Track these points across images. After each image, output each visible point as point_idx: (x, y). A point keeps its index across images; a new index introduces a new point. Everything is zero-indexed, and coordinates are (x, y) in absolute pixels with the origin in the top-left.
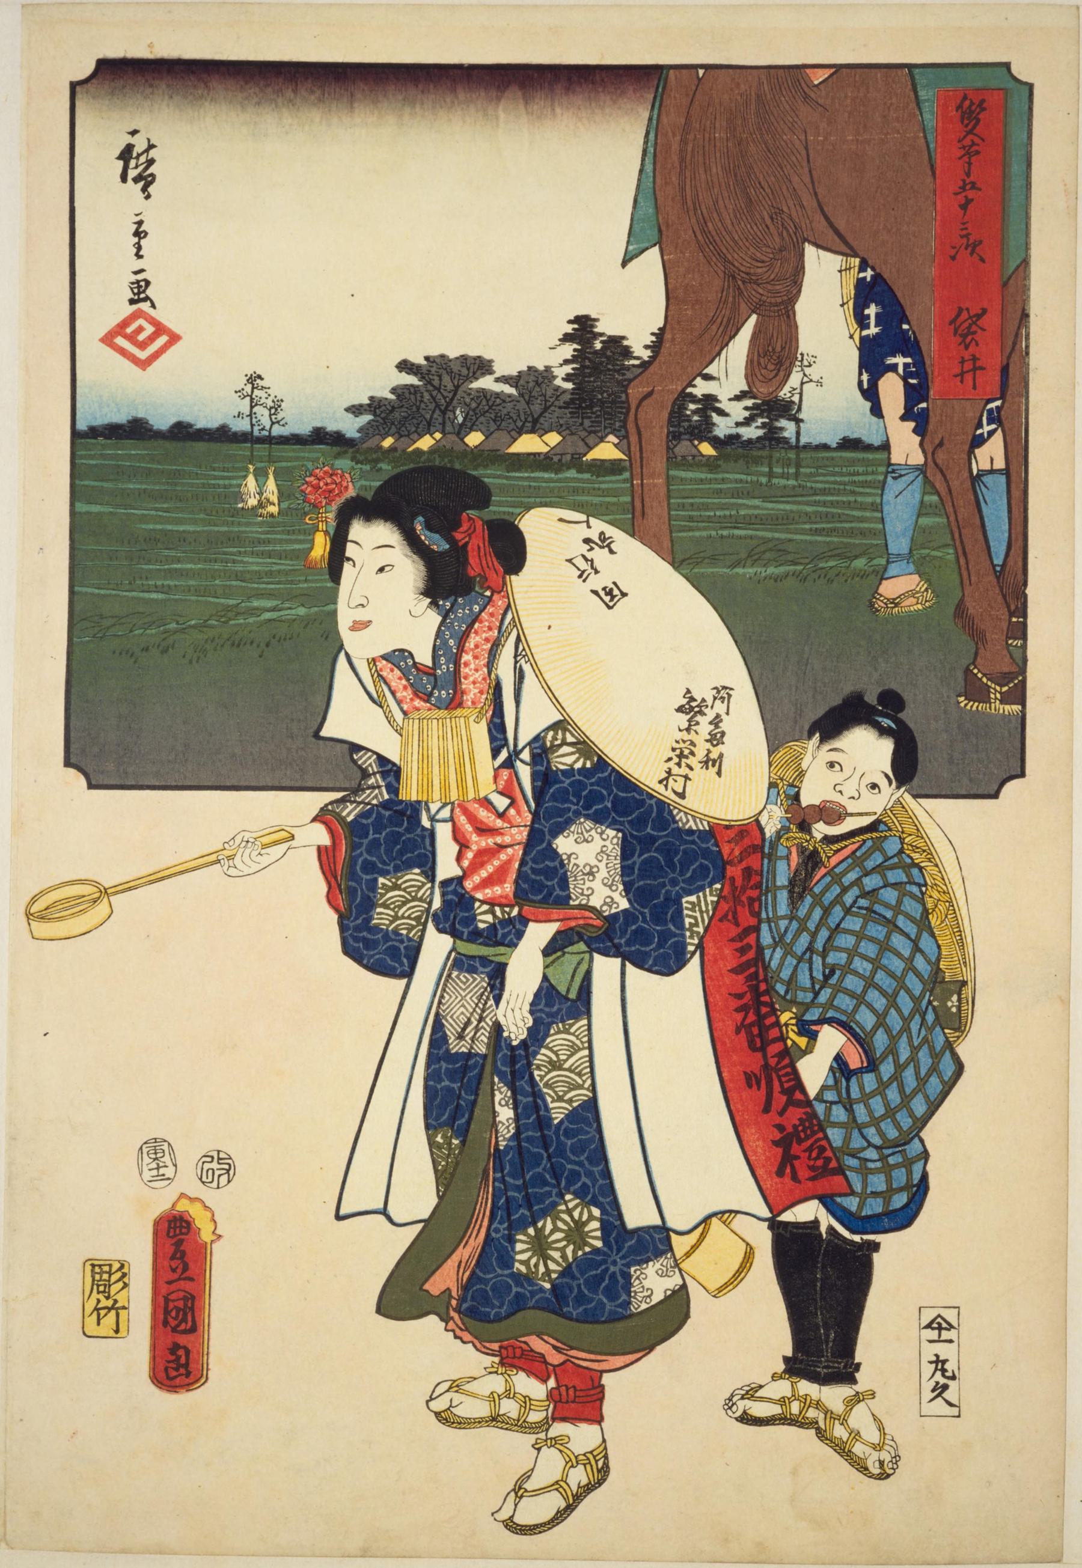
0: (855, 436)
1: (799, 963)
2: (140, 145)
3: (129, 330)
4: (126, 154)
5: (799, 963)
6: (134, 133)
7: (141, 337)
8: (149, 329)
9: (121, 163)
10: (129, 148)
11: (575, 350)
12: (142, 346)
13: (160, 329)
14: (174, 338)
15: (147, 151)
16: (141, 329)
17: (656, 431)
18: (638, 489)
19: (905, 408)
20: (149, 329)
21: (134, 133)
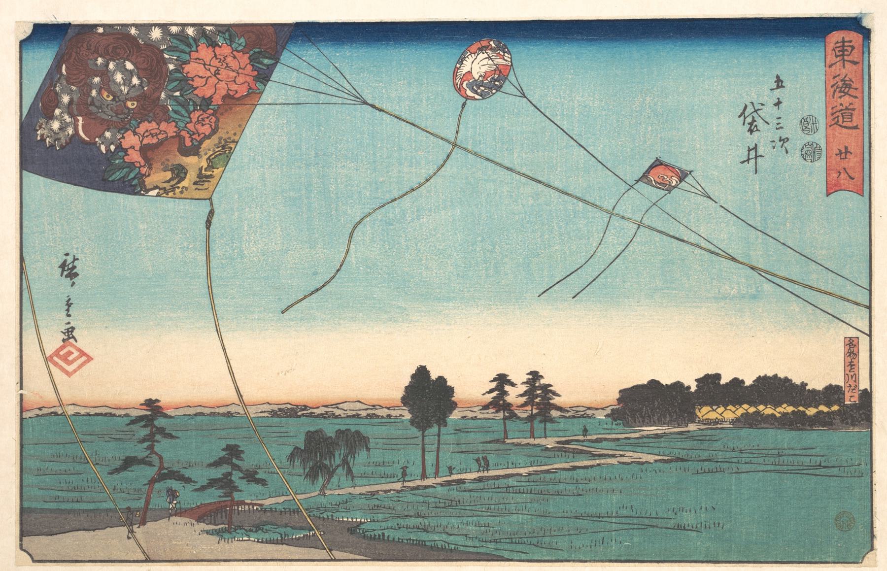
0: (674, 381)
1: (607, 211)
2: (70, 259)
3: (62, 353)
4: (63, 266)
5: (607, 211)
6: (67, 254)
7: (70, 358)
8: (76, 354)
9: (60, 270)
10: (65, 261)
11: (689, 388)
12: (69, 363)
13: (82, 353)
14: (90, 359)
15: (73, 262)
16: (70, 353)
17: (614, 485)
18: (609, 520)
19: (671, 385)
20: (76, 354)
21: (67, 254)
